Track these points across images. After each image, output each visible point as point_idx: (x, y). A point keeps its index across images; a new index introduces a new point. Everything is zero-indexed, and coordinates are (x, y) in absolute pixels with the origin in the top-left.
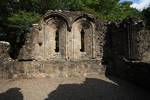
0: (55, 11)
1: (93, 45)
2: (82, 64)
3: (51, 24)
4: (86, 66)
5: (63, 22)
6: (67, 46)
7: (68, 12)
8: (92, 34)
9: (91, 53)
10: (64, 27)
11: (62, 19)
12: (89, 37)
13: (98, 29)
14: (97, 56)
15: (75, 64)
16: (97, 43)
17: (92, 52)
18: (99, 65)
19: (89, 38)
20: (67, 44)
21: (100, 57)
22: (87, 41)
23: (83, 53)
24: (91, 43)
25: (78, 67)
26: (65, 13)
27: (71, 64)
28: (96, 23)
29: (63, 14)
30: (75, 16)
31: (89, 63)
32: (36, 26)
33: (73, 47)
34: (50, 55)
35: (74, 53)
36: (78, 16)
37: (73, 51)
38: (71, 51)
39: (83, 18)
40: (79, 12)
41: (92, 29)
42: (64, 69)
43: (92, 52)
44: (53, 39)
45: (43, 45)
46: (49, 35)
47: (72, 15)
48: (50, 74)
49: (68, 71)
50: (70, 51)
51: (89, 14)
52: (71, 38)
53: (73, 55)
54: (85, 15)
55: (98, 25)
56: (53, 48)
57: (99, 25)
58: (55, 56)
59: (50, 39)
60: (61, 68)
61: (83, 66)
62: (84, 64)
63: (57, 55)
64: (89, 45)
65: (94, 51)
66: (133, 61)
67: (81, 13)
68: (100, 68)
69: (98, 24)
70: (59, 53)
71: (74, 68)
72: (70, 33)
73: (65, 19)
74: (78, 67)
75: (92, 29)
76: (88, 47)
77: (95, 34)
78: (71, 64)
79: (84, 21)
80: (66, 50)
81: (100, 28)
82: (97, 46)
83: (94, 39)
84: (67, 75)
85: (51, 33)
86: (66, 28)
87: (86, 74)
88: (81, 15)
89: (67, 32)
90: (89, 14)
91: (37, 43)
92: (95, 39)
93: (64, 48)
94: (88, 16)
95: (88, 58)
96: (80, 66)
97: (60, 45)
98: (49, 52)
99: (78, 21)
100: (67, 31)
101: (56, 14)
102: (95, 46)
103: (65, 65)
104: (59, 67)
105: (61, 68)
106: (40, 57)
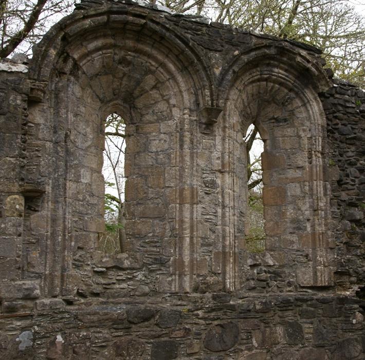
2: (277, 319)
3: (92, 72)
4: (295, 332)
11: (167, 56)
15: (242, 325)
18: (354, 321)
27: (216, 323)
36: (253, 54)
45: (46, 210)
46: (79, 144)
50: (209, 245)
51: (304, 53)
52: (213, 172)
61: (280, 330)
68: (356, 339)
69: (334, 105)
72: (206, 141)
77: (322, 154)
91: (16, 188)
99: (246, 78)
103: (188, 331)
104: (156, 346)
106: (28, 283)
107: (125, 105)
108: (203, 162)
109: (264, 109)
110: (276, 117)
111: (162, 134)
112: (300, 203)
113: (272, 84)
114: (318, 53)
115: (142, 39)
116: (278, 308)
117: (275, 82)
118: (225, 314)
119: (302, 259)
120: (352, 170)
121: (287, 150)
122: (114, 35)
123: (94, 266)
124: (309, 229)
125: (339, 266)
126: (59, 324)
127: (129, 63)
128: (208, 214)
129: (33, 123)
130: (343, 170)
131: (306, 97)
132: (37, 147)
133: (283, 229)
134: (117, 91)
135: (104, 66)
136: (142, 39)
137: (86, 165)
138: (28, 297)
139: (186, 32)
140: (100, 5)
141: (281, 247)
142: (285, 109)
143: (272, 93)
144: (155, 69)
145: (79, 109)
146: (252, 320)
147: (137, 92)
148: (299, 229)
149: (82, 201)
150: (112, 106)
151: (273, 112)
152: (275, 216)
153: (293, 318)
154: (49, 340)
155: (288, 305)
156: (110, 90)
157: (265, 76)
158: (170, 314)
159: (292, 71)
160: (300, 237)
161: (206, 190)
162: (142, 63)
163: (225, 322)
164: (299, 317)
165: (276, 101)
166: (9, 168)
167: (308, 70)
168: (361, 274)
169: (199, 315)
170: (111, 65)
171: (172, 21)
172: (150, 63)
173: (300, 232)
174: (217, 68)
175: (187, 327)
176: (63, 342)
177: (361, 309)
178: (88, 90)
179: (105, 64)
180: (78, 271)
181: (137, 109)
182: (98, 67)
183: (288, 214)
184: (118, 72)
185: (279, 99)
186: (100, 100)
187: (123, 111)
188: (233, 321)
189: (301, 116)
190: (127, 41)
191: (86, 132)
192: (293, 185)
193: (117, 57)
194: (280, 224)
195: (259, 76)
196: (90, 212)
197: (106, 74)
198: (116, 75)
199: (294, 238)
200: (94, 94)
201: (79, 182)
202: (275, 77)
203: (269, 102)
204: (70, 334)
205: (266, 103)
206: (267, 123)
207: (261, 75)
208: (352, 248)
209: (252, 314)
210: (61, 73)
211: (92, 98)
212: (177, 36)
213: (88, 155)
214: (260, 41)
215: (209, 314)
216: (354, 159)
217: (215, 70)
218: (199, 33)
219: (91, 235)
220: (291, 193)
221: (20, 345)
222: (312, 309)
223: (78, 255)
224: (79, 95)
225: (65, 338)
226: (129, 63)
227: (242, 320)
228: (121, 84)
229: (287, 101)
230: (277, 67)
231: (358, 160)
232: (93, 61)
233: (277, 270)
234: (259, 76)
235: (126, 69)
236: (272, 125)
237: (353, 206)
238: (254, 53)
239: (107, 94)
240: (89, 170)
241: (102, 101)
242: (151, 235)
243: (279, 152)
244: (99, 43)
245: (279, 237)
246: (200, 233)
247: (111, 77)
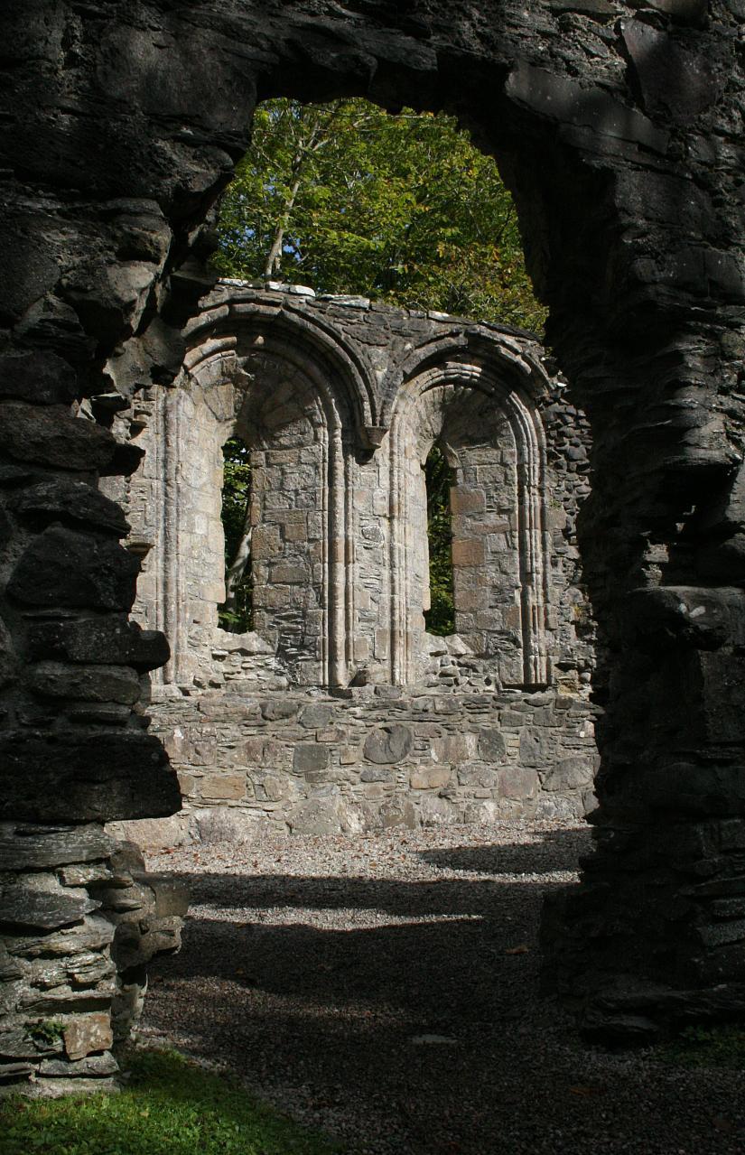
0: (268, 289)
1: (527, 577)
4: (491, 745)
5: (311, 379)
6: (340, 578)
7: (358, 308)
8: (521, 495)
9: (515, 641)
10: (318, 419)
12: (493, 516)
13: (561, 452)
14: (559, 666)
16: (555, 564)
17: (521, 640)
19: (493, 519)
20: (340, 566)
21: (582, 681)
22: (478, 547)
23: (442, 643)
24: (512, 563)
25: (433, 752)
26: (343, 316)
27: (381, 724)
28: (548, 404)
29: (326, 320)
30: (409, 346)
31: (511, 716)
33: (387, 588)
35: (401, 641)
37: (387, 626)
38: (378, 620)
39: (456, 360)
41: (521, 454)
42: (335, 771)
43: (521, 640)
47: (390, 335)
48: (224, 810)
49: (361, 786)
50: (369, 621)
51: (510, 340)
53: (387, 656)
54: (475, 339)
55: (559, 426)
57: (566, 423)
58: (222, 666)
60: (311, 764)
61: (471, 740)
62: (474, 731)
63: (238, 658)
64: (492, 574)
65: (541, 630)
66: (707, 323)
67: (455, 327)
69: (559, 415)
70: (252, 640)
71: (403, 756)
72: (362, 473)
73: (327, 361)
74: (433, 752)
75: (521, 454)
76: (489, 594)
78: (388, 725)
79: (467, 384)
80: (340, 613)
81: (576, 445)
82: (558, 591)
83: (539, 532)
84: (355, 816)
86: (339, 432)
87: (491, 806)
88: (453, 341)
89: (340, 465)
90: (510, 340)
92: (543, 530)
93: (313, 595)
94: (503, 350)
95: (492, 687)
96: (447, 743)
97: (270, 565)
100: (339, 454)
101: (276, 311)
102: (545, 586)
103: (341, 734)
105: (311, 764)
171: (314, 307)
199: (497, 614)
217: (378, 372)
225: (185, 734)
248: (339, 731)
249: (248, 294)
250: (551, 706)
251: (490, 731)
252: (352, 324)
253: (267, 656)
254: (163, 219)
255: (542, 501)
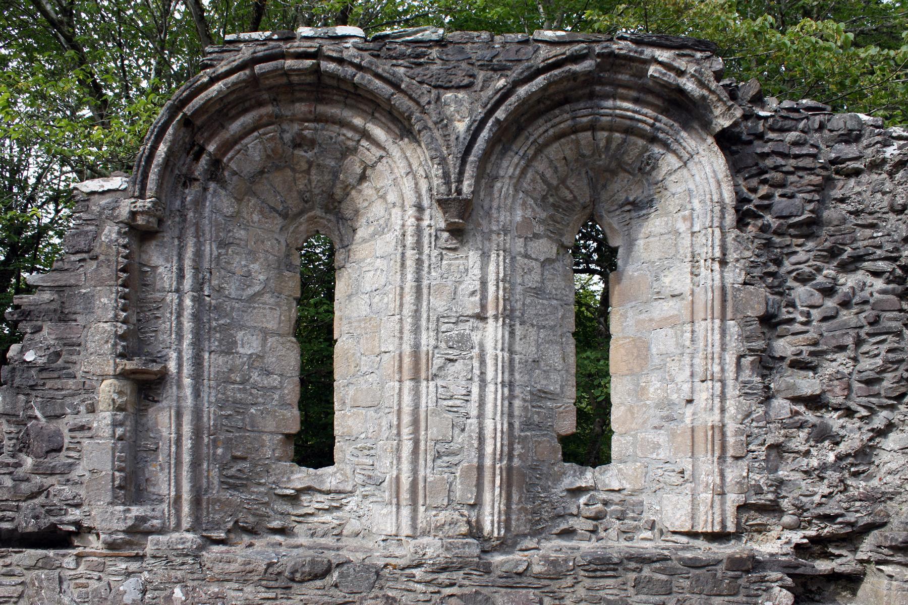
3: (248, 169)
29: (383, 67)
32: (104, 201)
34: (238, 497)
36: (541, 80)
40: (549, 34)
44: (272, 325)
51: (664, 55)
56: (271, 425)
59: (242, 327)
85: (255, 267)
98: (223, 467)
99: (540, 130)
107: (328, 216)
108: (444, 303)
109: (604, 186)
110: (631, 199)
111: (379, 260)
112: (673, 366)
113: (606, 134)
114: (701, 51)
115: (324, 96)
116: (582, 573)
117: (611, 129)
118: (467, 576)
119: (673, 479)
120: (801, 292)
121: (654, 262)
122: (275, 100)
123: (274, 486)
124: (688, 421)
125: (753, 492)
126: (179, 573)
127: (312, 143)
128: (451, 398)
129: (149, 267)
130: (781, 294)
131: (684, 148)
132: (155, 302)
133: (641, 421)
134: (308, 194)
135: (268, 156)
136: (324, 96)
137: (248, 324)
138: (135, 530)
139: (393, 65)
140: (236, 53)
141: (636, 455)
142: (647, 180)
143: (611, 152)
144: (354, 143)
145: (231, 234)
146: (524, 591)
147: (338, 192)
148: (670, 419)
149: (241, 384)
150: (307, 221)
151: (626, 191)
152: (629, 395)
153: (615, 592)
154: (163, 594)
155: (604, 568)
156: (295, 195)
157: (585, 119)
158: (359, 572)
159: (650, 98)
160: (673, 435)
161: (448, 354)
162: (331, 138)
163: (466, 591)
164: (631, 591)
165: (628, 168)
166: (102, 338)
167: (681, 91)
168: (808, 509)
169: (414, 577)
170: (280, 151)
171: (366, 50)
172: (344, 135)
173: (673, 425)
174: (459, 121)
175: (390, 594)
176: (184, 598)
177: (789, 581)
178: (249, 200)
179: (269, 152)
180: (236, 493)
181: (346, 220)
182: (258, 159)
183: (652, 390)
184: (298, 162)
185: (630, 162)
186: (280, 215)
187: (328, 228)
188: (485, 591)
189: (679, 190)
190: (297, 105)
191: (249, 271)
192: (663, 332)
193: (287, 136)
194: (636, 409)
195: (569, 122)
196: (260, 400)
197: (278, 168)
198: (297, 167)
199: (661, 438)
200: (265, 205)
201: (233, 353)
202: (609, 118)
203: (614, 173)
204: (194, 589)
205: (608, 175)
206: (617, 213)
207: (574, 118)
208: (793, 455)
209: (526, 580)
210: (188, 180)
211: (261, 212)
212: (378, 76)
213: (254, 308)
214: (559, 50)
215: (435, 576)
216: (809, 266)
217: (457, 124)
218: (422, 60)
219: (264, 437)
220: (658, 349)
221: (125, 597)
222: (664, 577)
223: (234, 470)
224: (229, 211)
225: (186, 594)
226: (312, 143)
227: (503, 590)
228: (310, 181)
229: (648, 164)
230: (614, 97)
231: (819, 270)
232: (246, 151)
233: (627, 498)
234: (569, 122)
235: (310, 153)
236: (627, 216)
237: (802, 369)
238: (542, 77)
239: (289, 202)
240: (257, 332)
241: (285, 216)
242: (363, 436)
243: (638, 270)
244: (247, 119)
245: (635, 436)
246: (433, 432)
247: (289, 172)
248: (388, 597)
249: (273, 48)
250: (722, 566)
251: (616, 601)
252: (420, 64)
253: (343, 496)
254: (708, 58)
255: (722, 278)
